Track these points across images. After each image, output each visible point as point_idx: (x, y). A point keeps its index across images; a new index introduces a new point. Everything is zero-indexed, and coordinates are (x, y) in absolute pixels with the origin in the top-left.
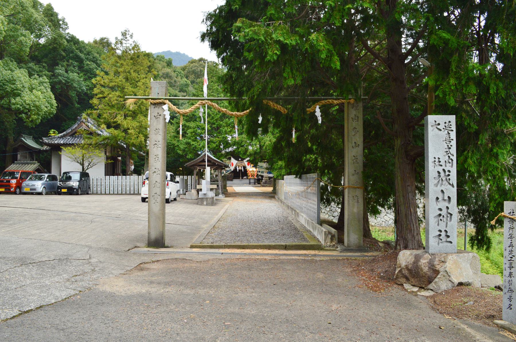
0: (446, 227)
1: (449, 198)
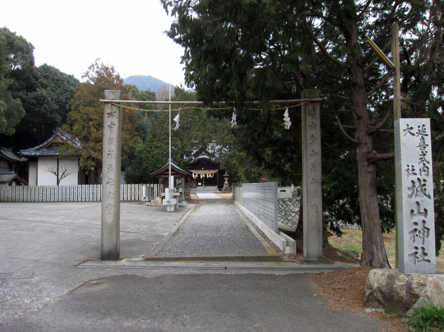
0: (423, 243)
1: (425, 210)
